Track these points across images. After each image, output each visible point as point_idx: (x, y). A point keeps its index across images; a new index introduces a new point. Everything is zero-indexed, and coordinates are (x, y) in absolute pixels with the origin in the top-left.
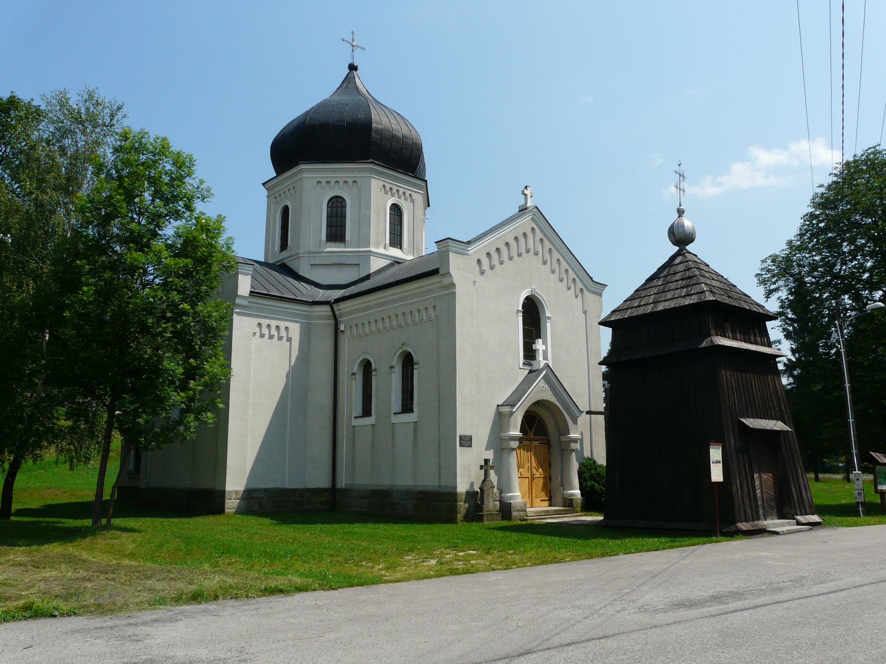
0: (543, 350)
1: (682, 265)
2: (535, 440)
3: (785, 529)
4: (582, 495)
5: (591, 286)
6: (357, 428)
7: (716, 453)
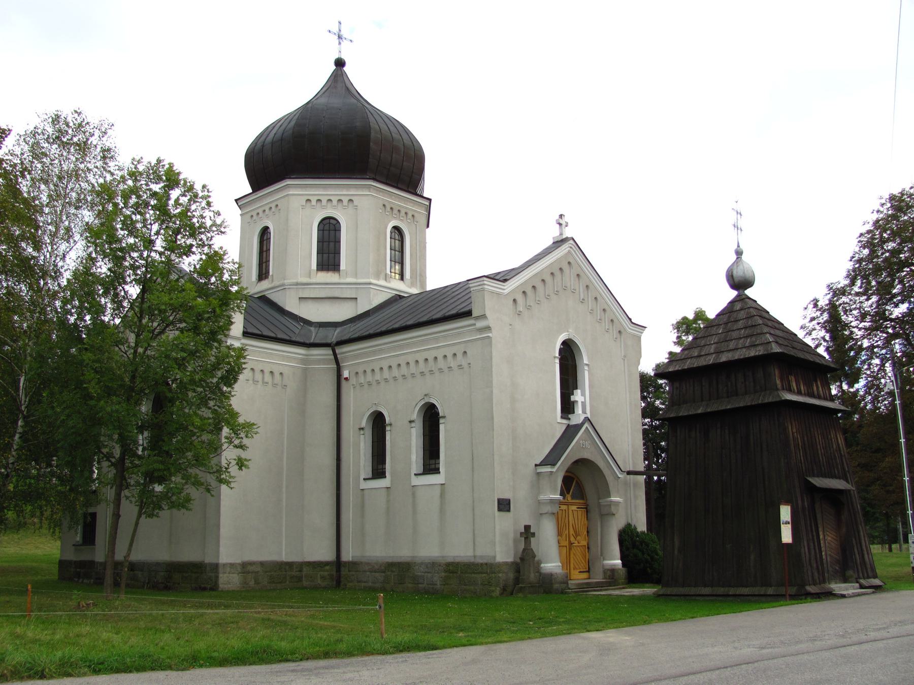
0: (582, 402)
1: (742, 312)
2: (573, 504)
3: (850, 592)
4: (624, 565)
5: (630, 329)
6: (366, 492)
7: (785, 513)
